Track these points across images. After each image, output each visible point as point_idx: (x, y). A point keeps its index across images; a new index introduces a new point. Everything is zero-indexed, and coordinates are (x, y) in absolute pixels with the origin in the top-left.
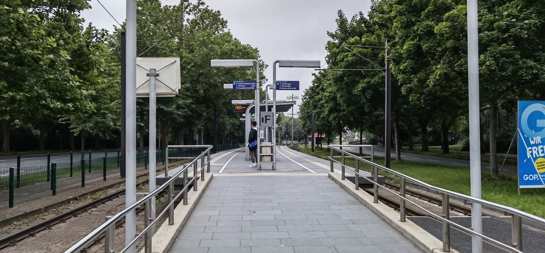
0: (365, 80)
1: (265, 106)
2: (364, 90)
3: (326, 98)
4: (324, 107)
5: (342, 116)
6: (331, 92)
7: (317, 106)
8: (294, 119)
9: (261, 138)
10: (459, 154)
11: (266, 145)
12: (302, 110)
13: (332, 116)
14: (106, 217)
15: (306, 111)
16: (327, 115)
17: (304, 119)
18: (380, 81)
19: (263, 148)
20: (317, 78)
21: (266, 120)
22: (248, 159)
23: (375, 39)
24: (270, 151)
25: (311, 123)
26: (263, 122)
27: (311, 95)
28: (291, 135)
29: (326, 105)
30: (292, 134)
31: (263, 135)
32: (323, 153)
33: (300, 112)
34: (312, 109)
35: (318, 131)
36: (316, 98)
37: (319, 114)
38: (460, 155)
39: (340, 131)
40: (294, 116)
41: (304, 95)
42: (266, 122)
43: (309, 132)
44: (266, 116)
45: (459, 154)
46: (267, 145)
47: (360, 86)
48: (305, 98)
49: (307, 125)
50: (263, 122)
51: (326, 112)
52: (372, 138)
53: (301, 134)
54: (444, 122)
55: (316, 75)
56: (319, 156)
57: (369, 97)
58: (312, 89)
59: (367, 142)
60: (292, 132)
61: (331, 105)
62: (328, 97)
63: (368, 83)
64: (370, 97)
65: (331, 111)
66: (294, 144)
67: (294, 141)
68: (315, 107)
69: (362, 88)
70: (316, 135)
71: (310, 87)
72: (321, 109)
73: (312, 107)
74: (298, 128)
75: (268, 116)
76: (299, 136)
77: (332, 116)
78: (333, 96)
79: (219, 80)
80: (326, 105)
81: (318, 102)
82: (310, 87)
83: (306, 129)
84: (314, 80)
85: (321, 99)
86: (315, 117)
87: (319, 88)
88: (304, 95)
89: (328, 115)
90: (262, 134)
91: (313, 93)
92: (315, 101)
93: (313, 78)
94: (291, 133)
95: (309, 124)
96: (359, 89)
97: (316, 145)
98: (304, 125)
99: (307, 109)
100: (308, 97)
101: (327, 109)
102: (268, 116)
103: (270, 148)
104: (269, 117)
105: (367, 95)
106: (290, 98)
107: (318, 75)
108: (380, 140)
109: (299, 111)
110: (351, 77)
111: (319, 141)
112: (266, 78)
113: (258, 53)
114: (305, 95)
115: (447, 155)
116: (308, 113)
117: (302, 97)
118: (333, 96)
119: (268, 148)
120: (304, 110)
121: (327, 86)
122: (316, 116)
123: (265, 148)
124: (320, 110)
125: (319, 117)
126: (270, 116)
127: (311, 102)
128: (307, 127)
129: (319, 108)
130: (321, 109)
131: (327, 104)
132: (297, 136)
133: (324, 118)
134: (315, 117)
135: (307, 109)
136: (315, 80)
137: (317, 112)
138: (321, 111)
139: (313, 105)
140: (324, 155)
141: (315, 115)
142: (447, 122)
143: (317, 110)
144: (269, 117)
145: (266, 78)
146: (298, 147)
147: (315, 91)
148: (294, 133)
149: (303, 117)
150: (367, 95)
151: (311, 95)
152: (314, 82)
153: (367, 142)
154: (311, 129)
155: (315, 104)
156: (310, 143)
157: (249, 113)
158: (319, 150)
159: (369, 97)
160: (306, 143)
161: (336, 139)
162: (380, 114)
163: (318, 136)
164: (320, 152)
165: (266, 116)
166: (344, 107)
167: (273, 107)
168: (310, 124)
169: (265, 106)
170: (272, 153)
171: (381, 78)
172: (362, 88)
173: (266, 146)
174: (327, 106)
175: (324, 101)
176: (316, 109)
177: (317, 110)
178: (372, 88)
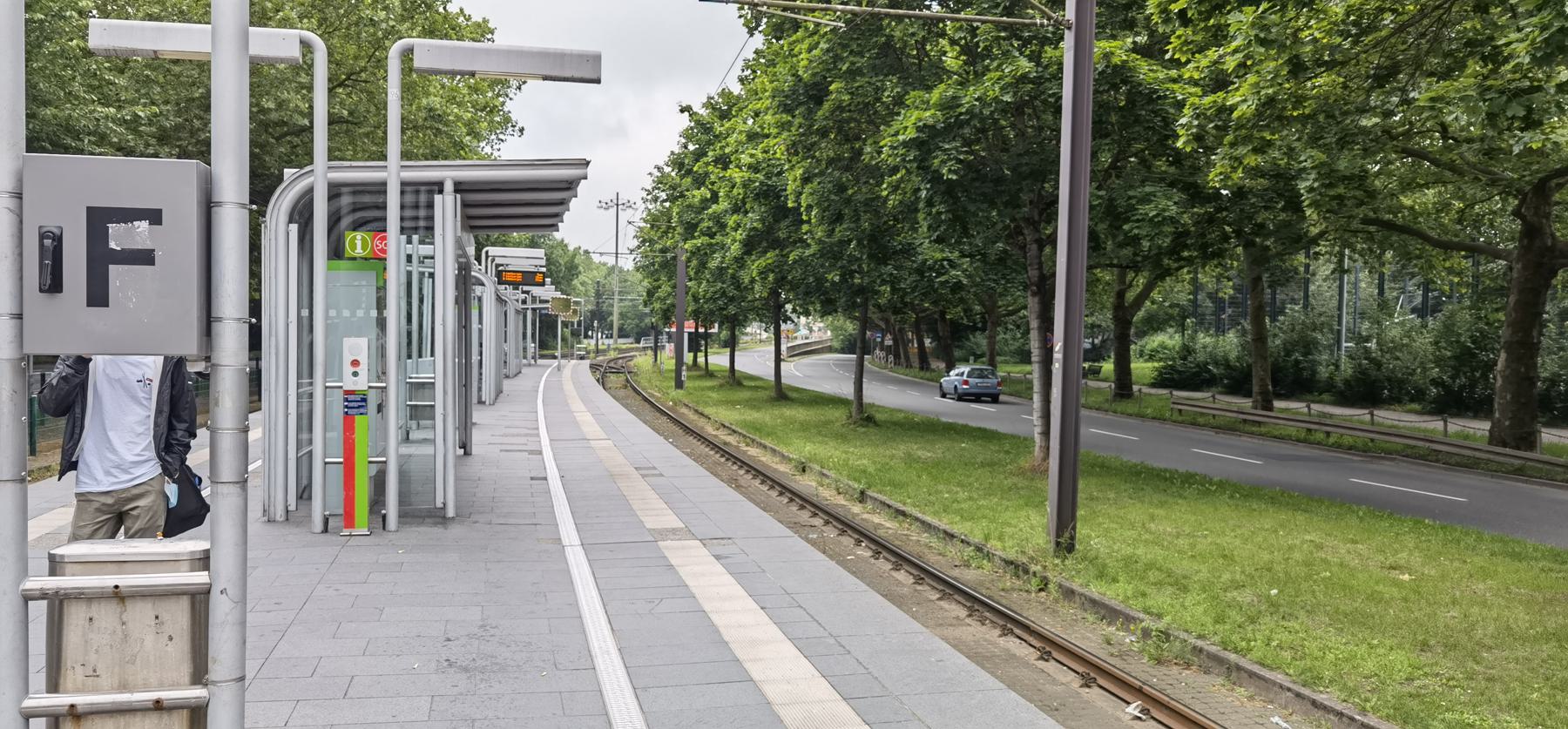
0: (935, 96)
1: (380, 188)
2: (926, 142)
3: (735, 191)
4: (723, 226)
5: (795, 262)
6: (754, 168)
7: (696, 226)
8: (621, 270)
9: (349, 383)
10: (1180, 407)
11: (108, 581)
12: (644, 241)
13: (755, 265)
14: (52, 552)
15: (658, 247)
16: (736, 259)
17: (652, 274)
18: (1007, 98)
19: (75, 617)
20: (698, 123)
21: (100, 259)
22: (279, 514)
23: (739, 194)
24: (178, 652)
25: (674, 287)
26: (53, 283)
27: (674, 189)
28: (612, 321)
29: (731, 221)
30: (615, 318)
31: (363, 369)
32: (714, 395)
33: (639, 247)
34: (677, 237)
35: (696, 315)
36: (694, 196)
37: (702, 255)
38: (1180, 411)
39: (774, 315)
40: (621, 263)
41: (650, 188)
42: (98, 296)
43: (666, 316)
44: (99, 220)
45: (1180, 407)
46: (127, 580)
47: (909, 123)
48: (656, 199)
49: (661, 293)
50: (53, 283)
51: (735, 249)
52: (850, 335)
53: (641, 320)
54: (1121, 295)
55: (696, 113)
56: (700, 409)
57: (950, 171)
58: (678, 162)
59: (836, 344)
60: (616, 311)
61: (753, 219)
62: (745, 185)
63: (949, 105)
64: (955, 172)
65: (750, 246)
66: (621, 351)
67: (621, 341)
68: (690, 229)
69: (919, 129)
70: (689, 327)
71: (672, 153)
72: (712, 236)
73: (679, 230)
74: (632, 300)
75: (128, 215)
76: (637, 326)
77: (755, 265)
78: (762, 183)
79: (300, 104)
80: (731, 221)
81: (700, 213)
82: (672, 153)
83: (657, 306)
84: (687, 130)
85: (715, 198)
86: (688, 267)
87: (705, 159)
88: (650, 188)
89: (740, 262)
90: (355, 363)
91: (682, 177)
92: (689, 206)
93: (685, 121)
94: (611, 314)
95: (666, 289)
96: (901, 138)
97: (688, 357)
98: (650, 293)
99: (660, 238)
100: (663, 196)
101: (740, 235)
102: (128, 215)
103: (178, 616)
104: (140, 234)
105: (943, 162)
106: (610, 204)
107: (703, 112)
108: (883, 341)
109: (636, 243)
110: (860, 81)
111: (696, 342)
112: (520, 125)
113: (489, 36)
114: (654, 189)
115: (1130, 407)
116: (664, 251)
117: (644, 194)
118: (762, 183)
119: (141, 614)
120: (652, 242)
121: (740, 143)
122: (694, 263)
123: (106, 614)
124: (706, 239)
125: (703, 265)
126: (155, 217)
127: (675, 210)
128: (659, 298)
129: (704, 235)
130: (712, 236)
131: (735, 217)
132: (630, 325)
133: (721, 270)
134: (688, 267)
135: (660, 238)
136: (692, 128)
137: (698, 249)
138: (711, 245)
139: (681, 222)
140: (718, 403)
141: (689, 260)
142: (1131, 295)
143: (698, 242)
144: (140, 234)
145: (520, 125)
146: (632, 363)
147: (689, 172)
148: (621, 314)
149: (647, 266)
150: (943, 162)
151: (674, 189)
152: (688, 135)
153: (836, 344)
154: (673, 305)
155: (689, 216)
156: (670, 348)
157: (291, 221)
158: (700, 377)
159: (950, 171)
160: (656, 349)
161: (747, 334)
162: (944, 259)
163: (697, 328)
164: (703, 389)
165: (99, 220)
166: (815, 230)
167: (441, 192)
168: (669, 289)
169: (380, 188)
170: (199, 675)
171: (1010, 84)
172: (919, 129)
173: (118, 596)
174: (738, 226)
175: (723, 205)
176: (693, 238)
177: (698, 242)
178: (967, 131)
